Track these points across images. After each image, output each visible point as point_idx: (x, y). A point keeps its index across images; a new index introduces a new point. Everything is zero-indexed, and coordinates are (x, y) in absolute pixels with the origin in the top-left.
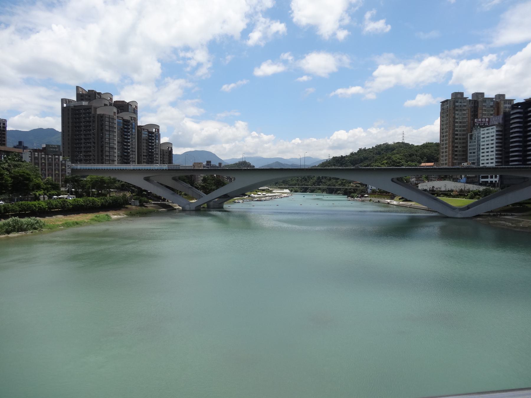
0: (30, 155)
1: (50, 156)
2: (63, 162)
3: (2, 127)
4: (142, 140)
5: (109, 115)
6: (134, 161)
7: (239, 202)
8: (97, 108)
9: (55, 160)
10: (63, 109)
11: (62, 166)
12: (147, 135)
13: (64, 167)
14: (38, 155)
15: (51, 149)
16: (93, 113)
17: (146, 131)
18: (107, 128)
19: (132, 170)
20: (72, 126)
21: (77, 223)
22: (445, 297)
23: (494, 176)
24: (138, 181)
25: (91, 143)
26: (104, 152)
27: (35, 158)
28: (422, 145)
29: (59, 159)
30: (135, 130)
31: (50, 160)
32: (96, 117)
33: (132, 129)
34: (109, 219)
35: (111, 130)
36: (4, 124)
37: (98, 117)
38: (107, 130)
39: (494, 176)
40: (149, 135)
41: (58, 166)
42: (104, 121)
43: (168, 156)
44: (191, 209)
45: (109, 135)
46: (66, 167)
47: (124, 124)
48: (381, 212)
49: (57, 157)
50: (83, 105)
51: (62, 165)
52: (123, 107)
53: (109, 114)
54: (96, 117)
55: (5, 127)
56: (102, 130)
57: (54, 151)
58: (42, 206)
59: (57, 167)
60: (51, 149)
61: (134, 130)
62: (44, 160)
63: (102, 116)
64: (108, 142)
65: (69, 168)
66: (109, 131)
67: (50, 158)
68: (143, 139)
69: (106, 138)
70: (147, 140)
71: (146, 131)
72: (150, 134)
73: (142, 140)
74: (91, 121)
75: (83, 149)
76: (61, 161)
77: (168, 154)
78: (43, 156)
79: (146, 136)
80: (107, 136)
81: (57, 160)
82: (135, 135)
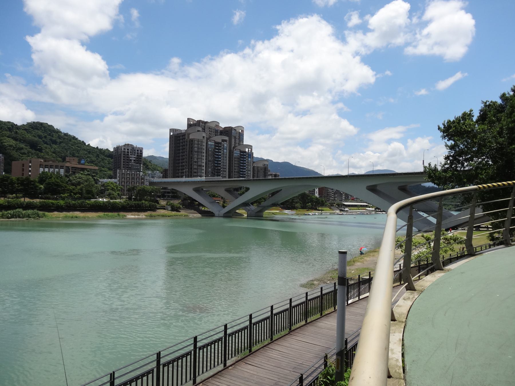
0: (119, 172)
1: (133, 172)
2: (143, 177)
3: (139, 153)
4: (234, 159)
5: (198, 139)
6: (226, 177)
7: (309, 215)
8: (190, 134)
9: (137, 176)
10: (171, 137)
11: (141, 180)
12: (239, 154)
13: (143, 181)
14: (125, 171)
15: (135, 167)
16: (186, 138)
17: (238, 151)
18: (196, 149)
19: (184, 182)
20: (174, 150)
21: (76, 217)
22: (239, 306)
23: (140, 157)
24: (189, 192)
25: (184, 162)
26: (193, 169)
27: (122, 174)
28: (58, 132)
29: (140, 175)
30: (227, 150)
31: (133, 175)
32: (188, 142)
33: (224, 149)
34: (124, 217)
35: (199, 152)
36: (141, 151)
37: (189, 141)
38: (196, 152)
39: (140, 157)
40: (241, 155)
41: (139, 179)
42: (194, 145)
43: (264, 172)
44: (220, 215)
45: (198, 155)
46: (144, 180)
47: (215, 146)
48: (307, 218)
49: (138, 173)
50: (182, 132)
51: (142, 179)
52: (227, 131)
53: (198, 138)
54: (188, 142)
55: (142, 154)
56: (192, 152)
57: (137, 168)
58: (60, 204)
59: (138, 180)
60: (135, 167)
61: (225, 151)
62: (129, 175)
63: (192, 141)
64: (197, 161)
65: (147, 181)
66: (198, 152)
67: (133, 174)
68: (234, 158)
69: (194, 158)
70: (238, 158)
71: (238, 151)
72: (241, 153)
73: (234, 159)
74: (185, 145)
75: (180, 168)
76: (141, 176)
77: (263, 170)
78: (128, 172)
79: (238, 155)
80: (196, 156)
81: (138, 175)
82: (226, 154)
